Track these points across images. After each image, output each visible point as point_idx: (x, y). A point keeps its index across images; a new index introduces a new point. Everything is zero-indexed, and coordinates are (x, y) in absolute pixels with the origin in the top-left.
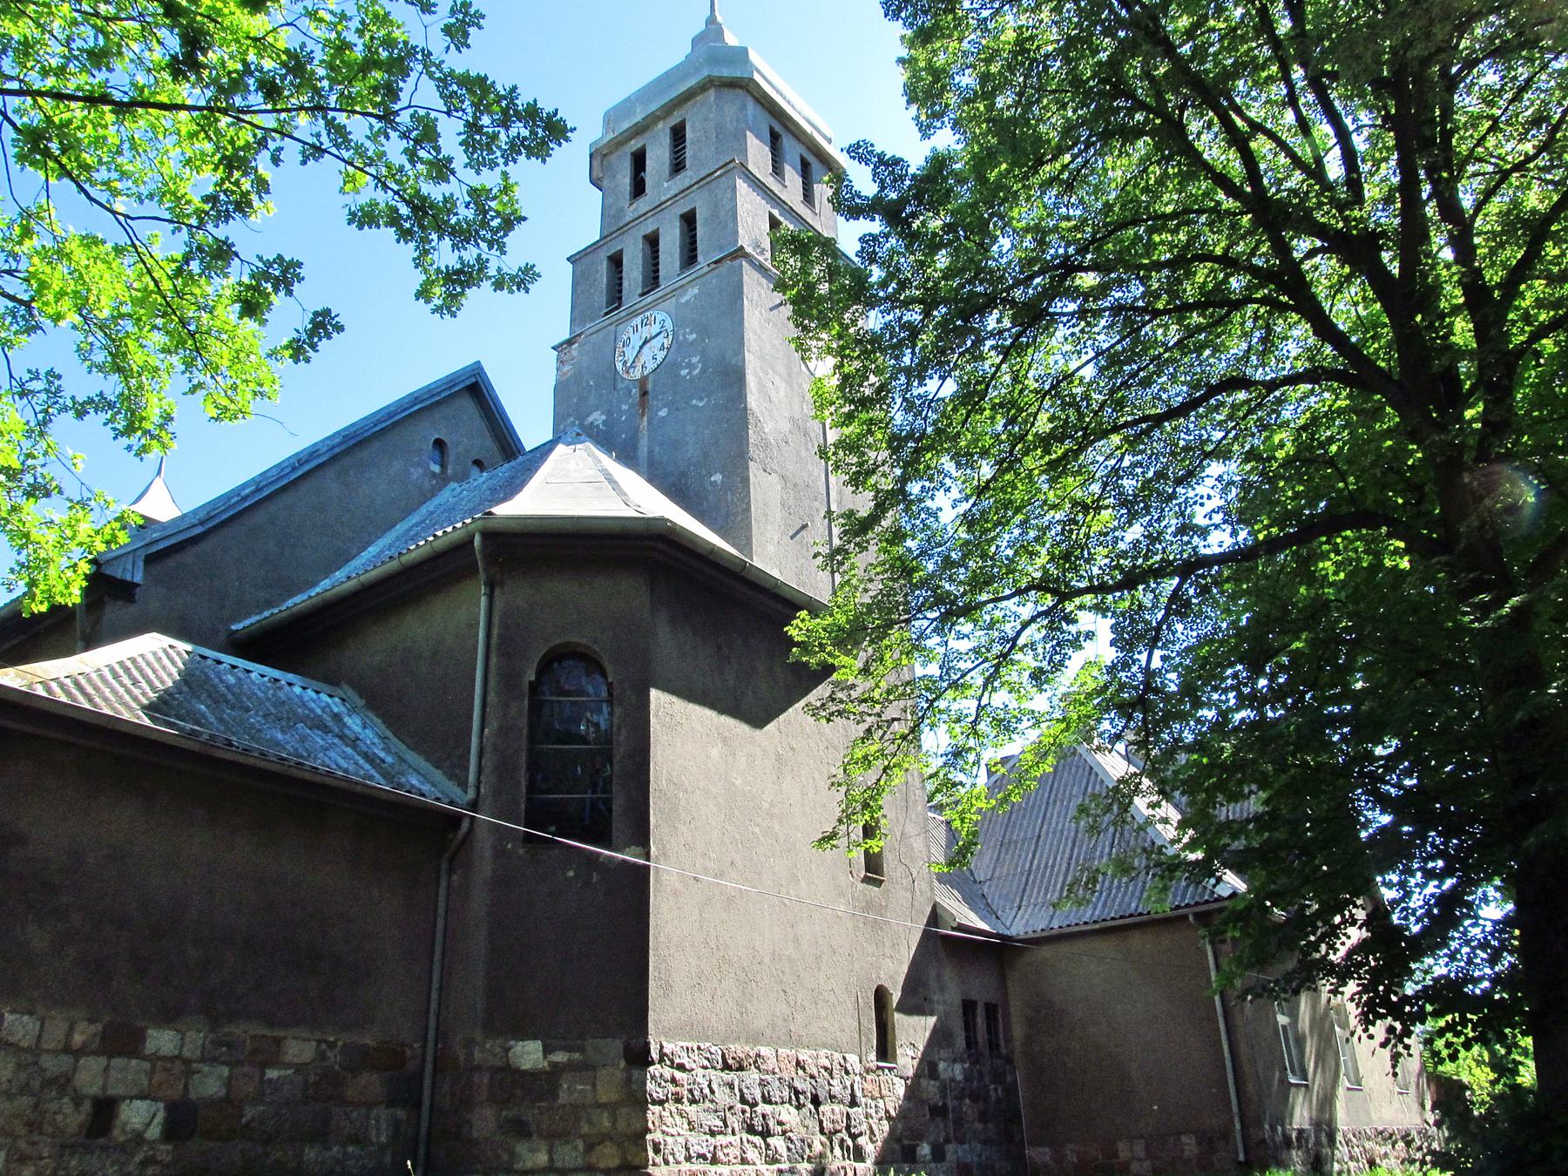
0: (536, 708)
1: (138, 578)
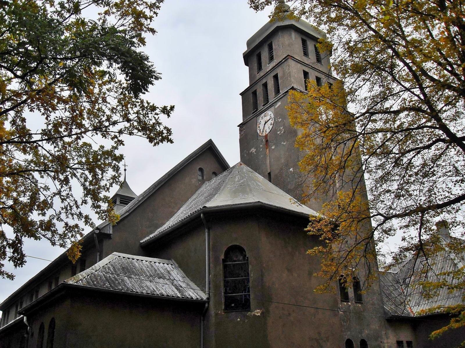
0: (225, 267)
1: (111, 232)
